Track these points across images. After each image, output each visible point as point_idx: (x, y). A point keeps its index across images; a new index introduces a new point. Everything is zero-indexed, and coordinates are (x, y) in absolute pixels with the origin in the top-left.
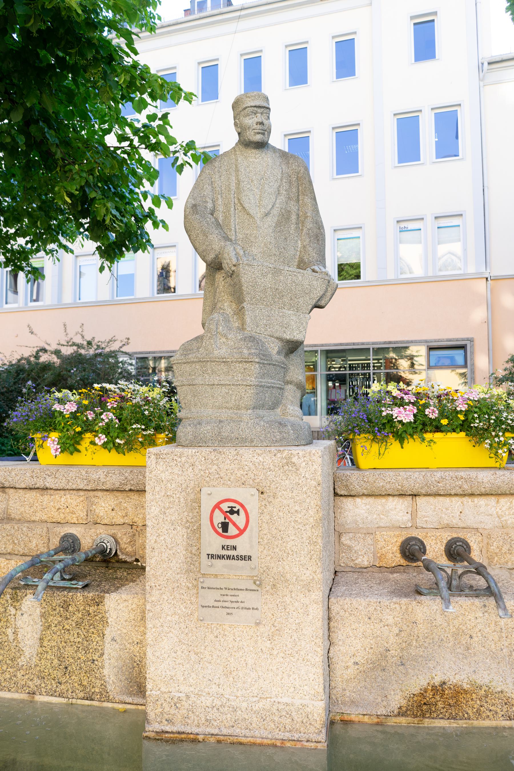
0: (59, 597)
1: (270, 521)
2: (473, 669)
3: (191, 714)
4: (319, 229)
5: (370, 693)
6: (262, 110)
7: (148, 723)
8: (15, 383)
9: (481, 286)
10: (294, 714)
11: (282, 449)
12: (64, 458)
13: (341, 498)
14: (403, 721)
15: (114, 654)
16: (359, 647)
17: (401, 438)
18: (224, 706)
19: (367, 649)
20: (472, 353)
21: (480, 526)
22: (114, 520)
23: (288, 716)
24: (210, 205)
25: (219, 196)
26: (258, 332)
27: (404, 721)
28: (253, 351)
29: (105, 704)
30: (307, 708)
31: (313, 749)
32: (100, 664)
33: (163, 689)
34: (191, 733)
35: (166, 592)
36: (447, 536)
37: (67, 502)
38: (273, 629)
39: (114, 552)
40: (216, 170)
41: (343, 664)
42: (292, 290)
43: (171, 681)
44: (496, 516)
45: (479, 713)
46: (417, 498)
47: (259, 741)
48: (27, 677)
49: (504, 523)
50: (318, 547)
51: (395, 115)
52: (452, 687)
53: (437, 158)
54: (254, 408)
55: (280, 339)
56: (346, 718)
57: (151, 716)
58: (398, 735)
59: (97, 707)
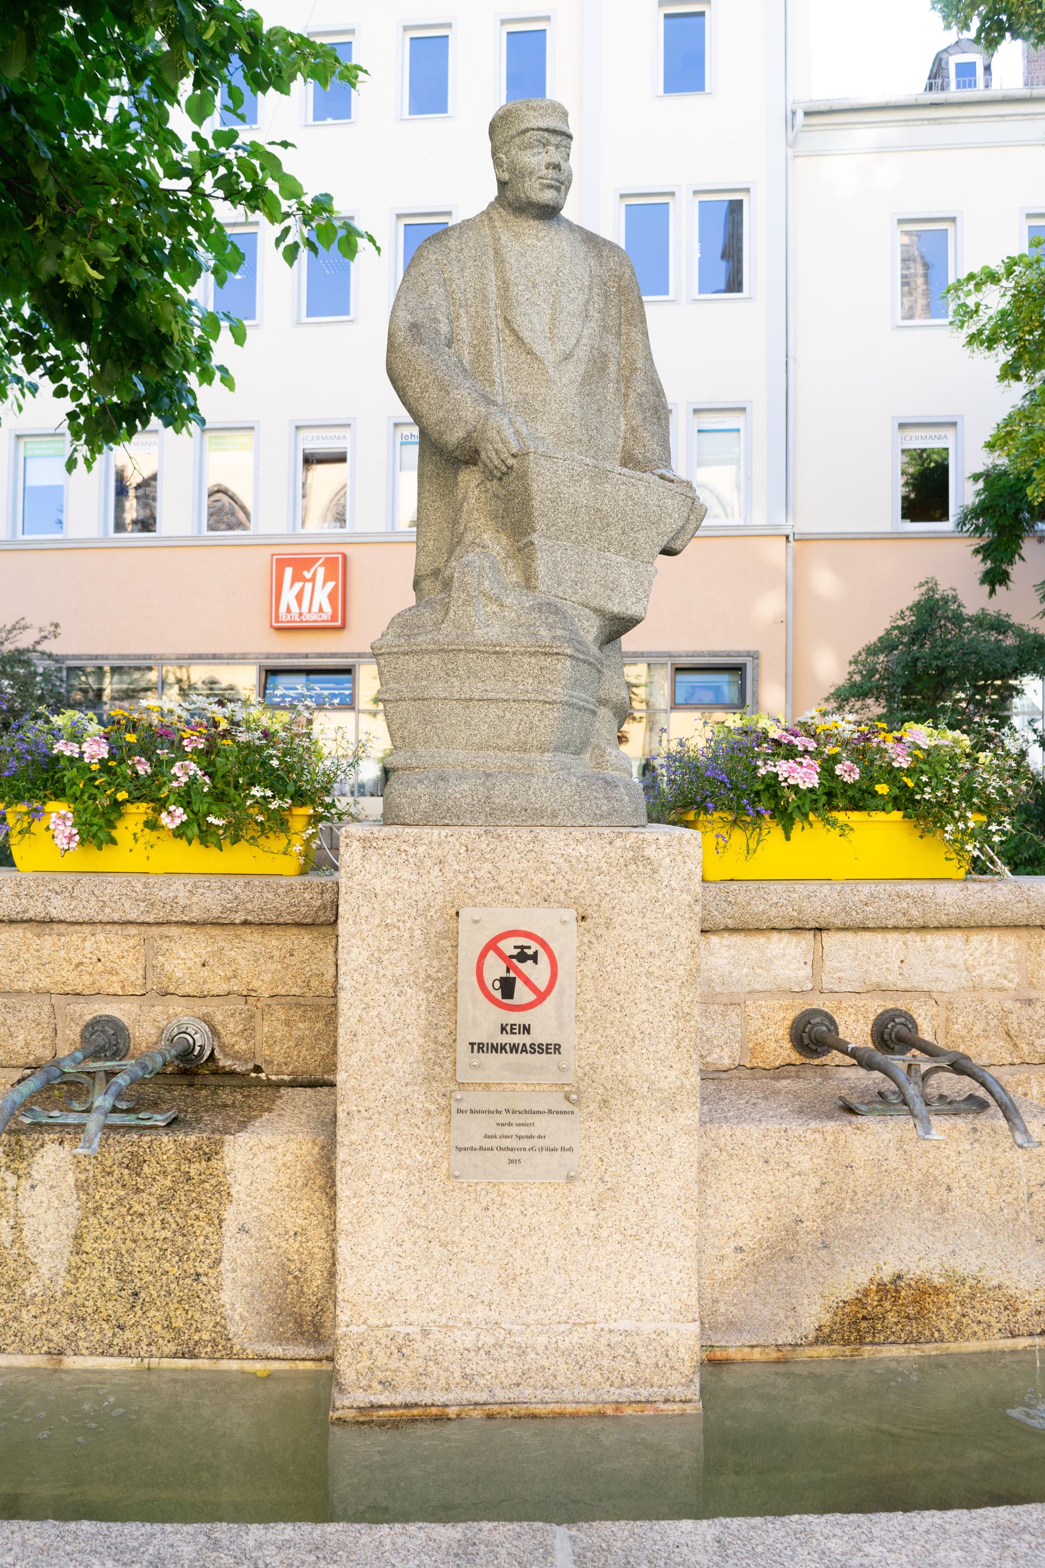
0: (122, 1147)
1: (598, 974)
2: (951, 1247)
3: (432, 1367)
4: (658, 395)
6: (559, 138)
7: (341, 1391)
9: (776, 552)
10: (640, 1351)
14: (824, 1351)
15: (244, 1259)
16: (746, 1219)
17: (785, 817)
18: (501, 1347)
19: (761, 1221)
20: (756, 680)
22: (206, 987)
23: (628, 1356)
26: (561, 595)
28: (559, 633)
30: (666, 1339)
31: (678, 1415)
32: (213, 1282)
33: (373, 1321)
34: (433, 1405)
35: (383, 1124)
36: (876, 1006)
37: (98, 948)
38: (601, 1188)
39: (207, 1053)
40: (453, 255)
41: (715, 1253)
42: (625, 514)
43: (391, 1303)
44: (963, 967)
45: (959, 1327)
46: (824, 934)
47: (570, 1408)
48: (44, 1319)
49: (977, 980)
50: (693, 1023)
51: (622, 196)
52: (913, 1283)
53: (701, 292)
55: (599, 612)
56: (719, 1354)
58: (817, 1380)
59: (205, 1371)
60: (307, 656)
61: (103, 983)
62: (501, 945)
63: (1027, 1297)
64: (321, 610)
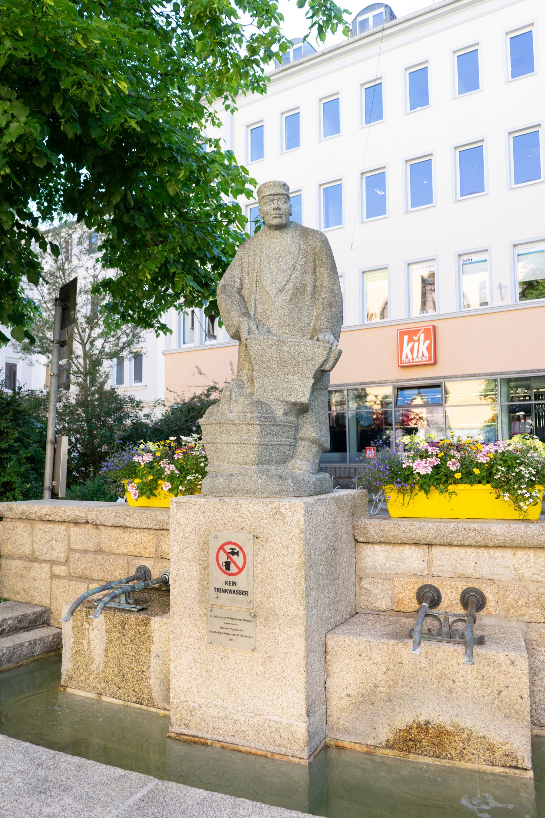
0: (119, 617)
3: (202, 722)
5: (362, 724)
8: (186, 421)
10: (281, 731)
11: (272, 500)
12: (143, 501)
13: (362, 545)
14: (390, 753)
16: (351, 681)
21: (496, 578)
24: (237, 284)
25: (246, 275)
27: (391, 754)
28: (255, 415)
29: (152, 709)
33: (182, 698)
36: (463, 586)
38: (265, 656)
42: (295, 358)
44: (512, 568)
45: (461, 755)
47: (254, 751)
48: (96, 680)
54: (258, 464)
56: (340, 743)
57: (173, 720)
60: (417, 380)
61: (142, 552)
62: (225, 547)
63: (500, 746)
64: (423, 355)
